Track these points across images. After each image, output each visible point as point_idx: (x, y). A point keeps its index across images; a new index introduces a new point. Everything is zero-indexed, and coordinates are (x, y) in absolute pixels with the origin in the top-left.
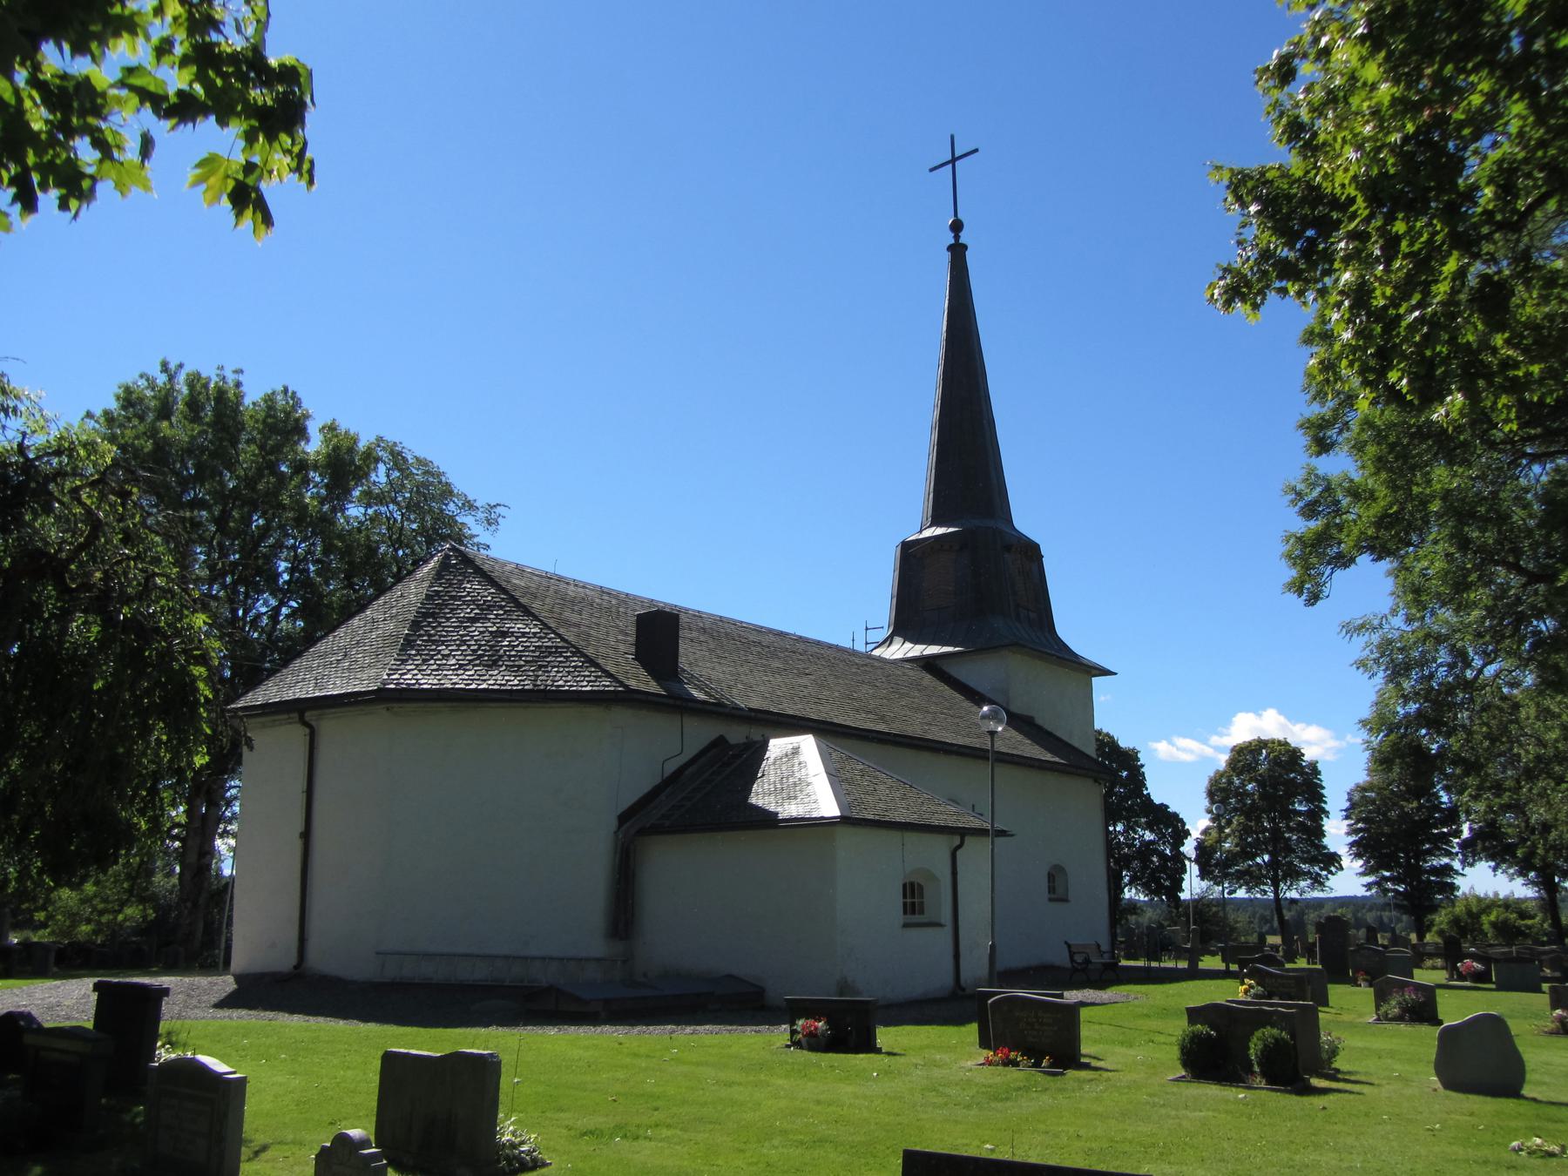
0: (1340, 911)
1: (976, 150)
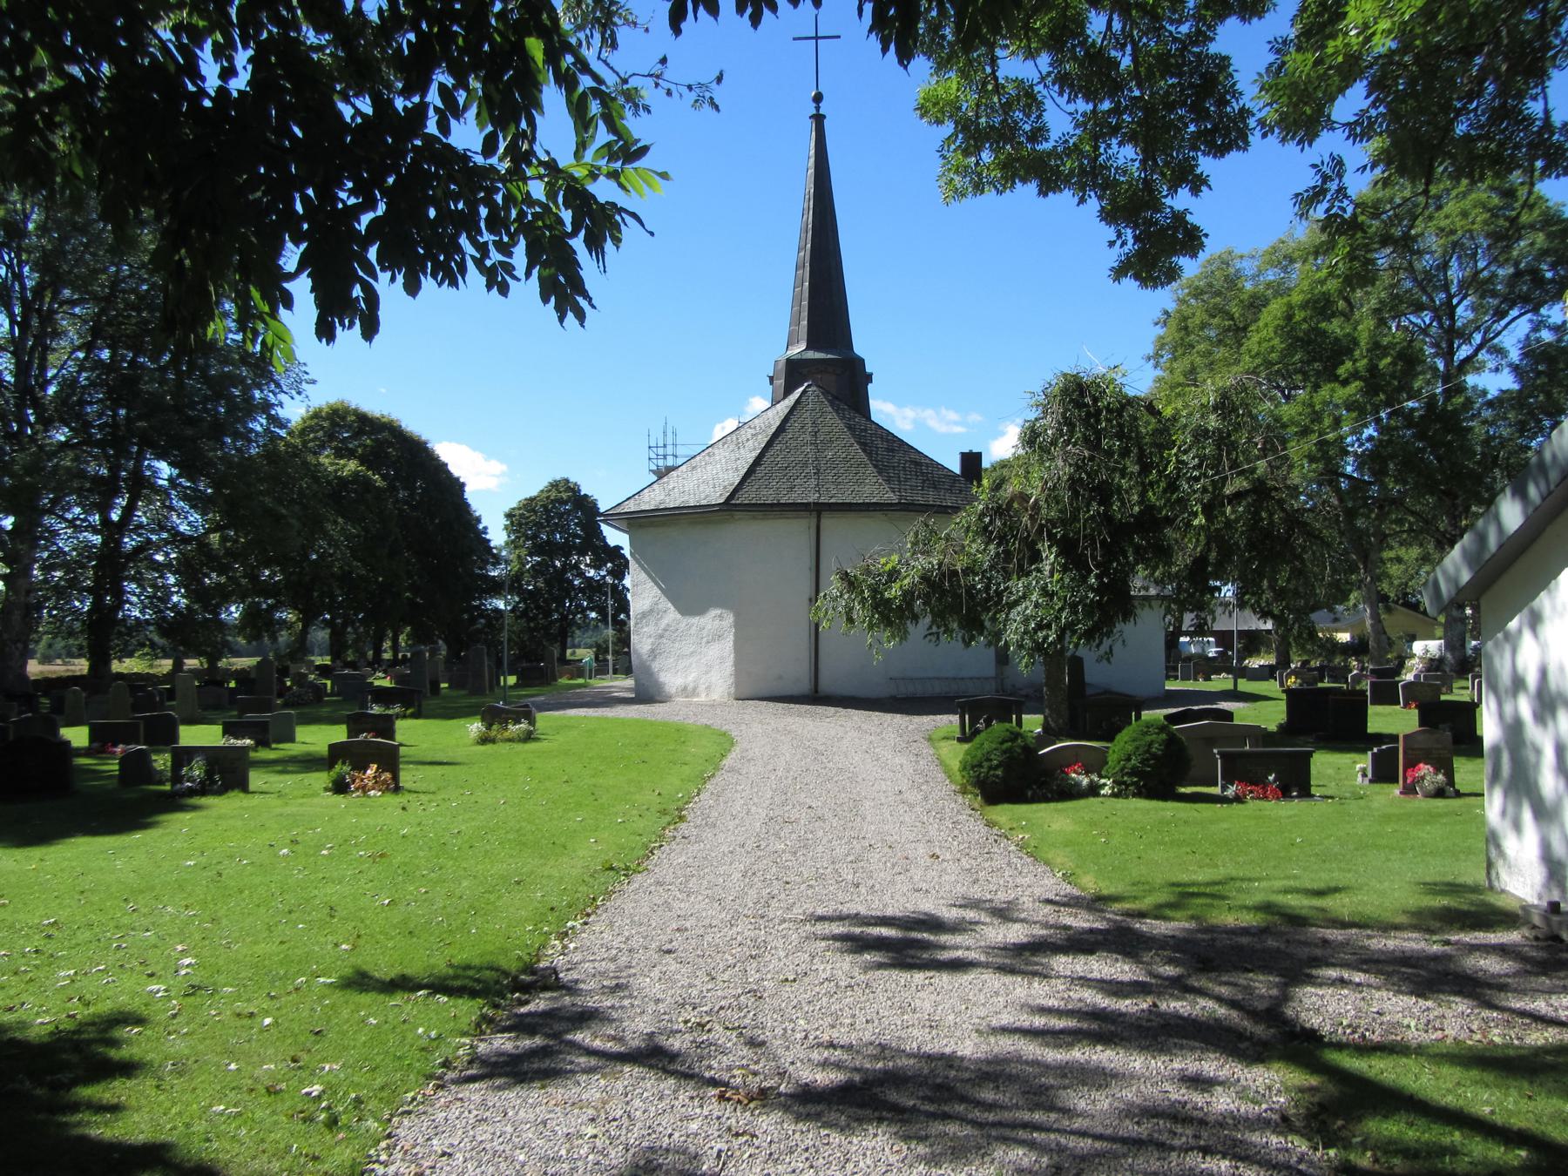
0: (1288, 411)
1: (839, 37)
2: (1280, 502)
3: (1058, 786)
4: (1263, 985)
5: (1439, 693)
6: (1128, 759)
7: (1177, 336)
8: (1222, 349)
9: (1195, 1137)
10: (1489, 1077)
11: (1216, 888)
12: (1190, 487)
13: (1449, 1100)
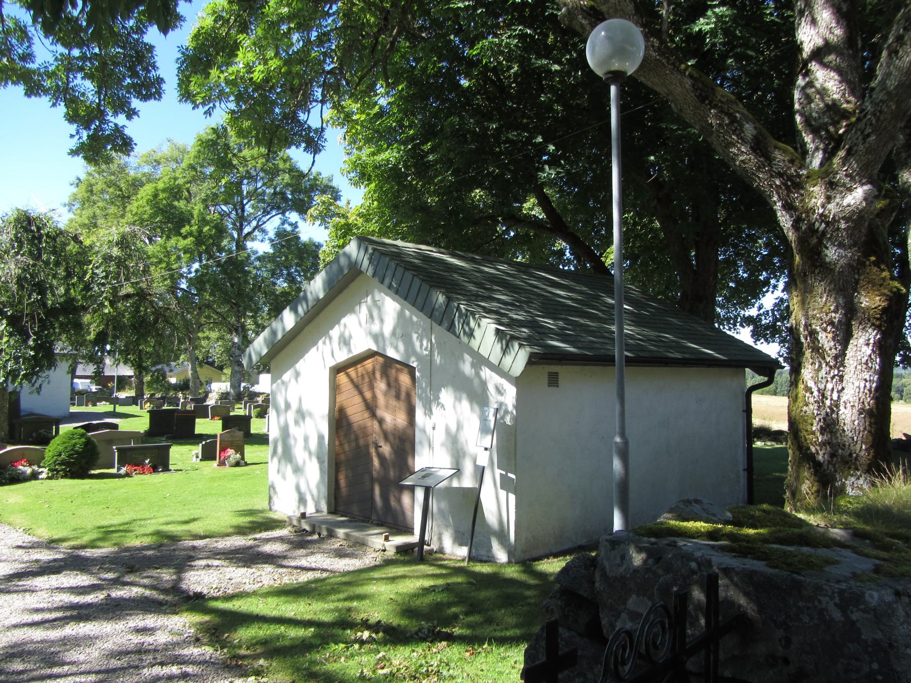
2: (152, 302)
3: (9, 474)
4: (167, 575)
5: (229, 412)
6: (60, 455)
7: (86, 195)
8: (113, 207)
9: (154, 659)
10: (290, 598)
11: (126, 526)
12: (99, 289)
13: (275, 613)
